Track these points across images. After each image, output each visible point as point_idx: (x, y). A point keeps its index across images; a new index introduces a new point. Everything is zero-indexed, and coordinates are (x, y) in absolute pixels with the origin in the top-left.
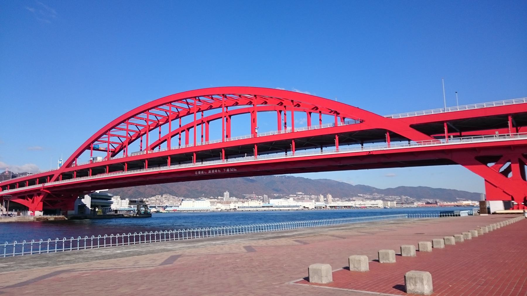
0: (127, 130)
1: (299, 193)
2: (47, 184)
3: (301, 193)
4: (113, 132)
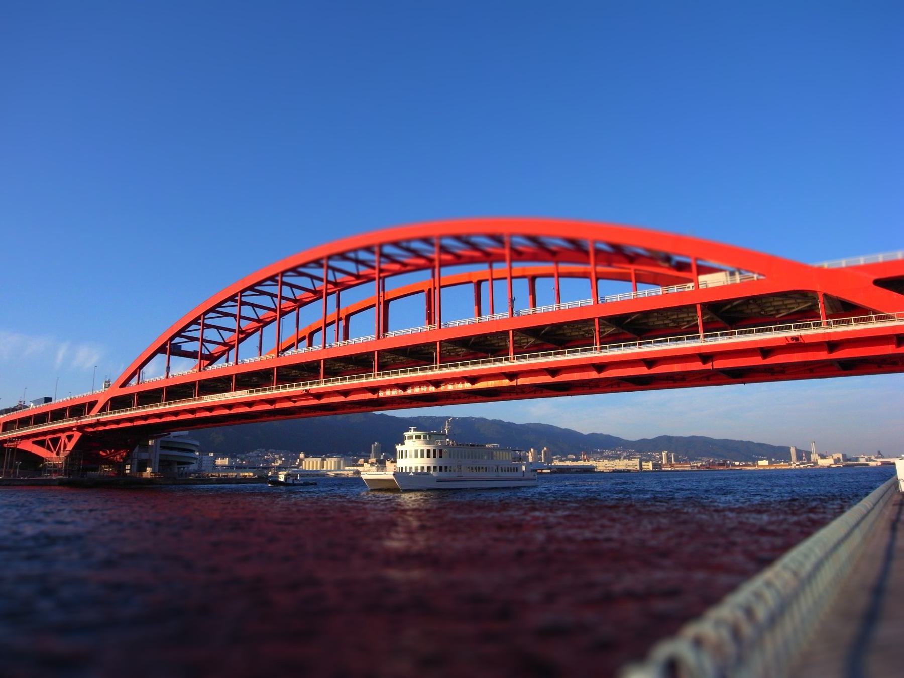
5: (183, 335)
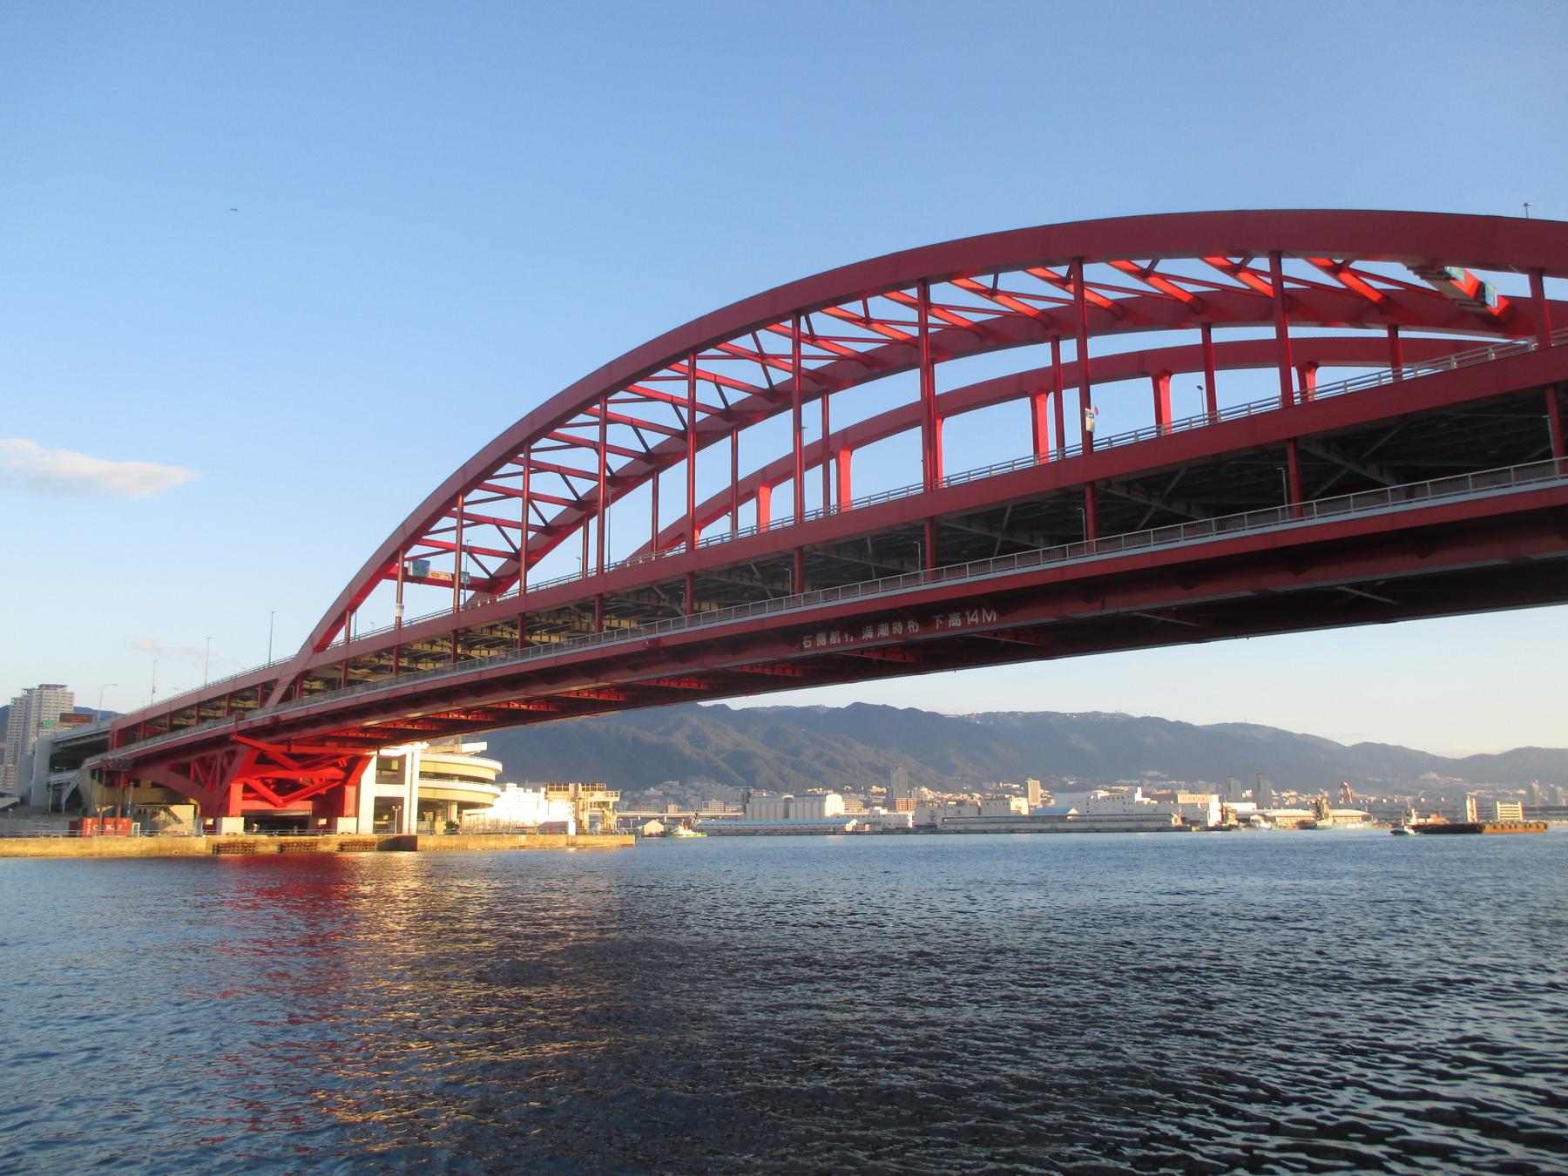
0: (602, 447)
1: (1150, 773)
2: (968, 1123)
5: (559, 434)
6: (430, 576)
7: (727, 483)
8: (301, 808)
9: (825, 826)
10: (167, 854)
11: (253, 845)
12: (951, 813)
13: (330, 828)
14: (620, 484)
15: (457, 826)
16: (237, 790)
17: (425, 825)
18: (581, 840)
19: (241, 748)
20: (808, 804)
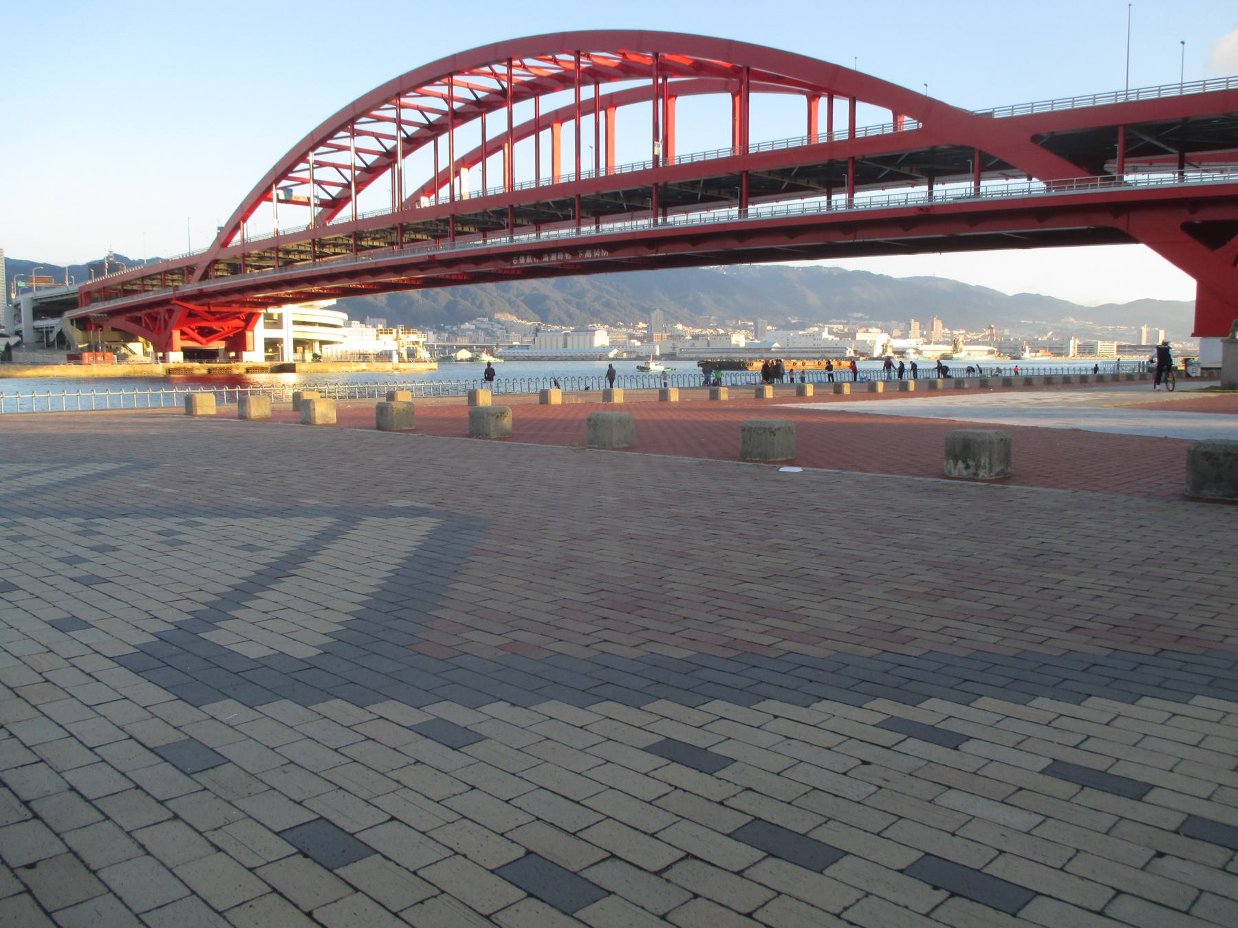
0: (399, 122)
3: (860, 315)
4: (363, 125)
6: (294, 199)
7: (479, 143)
8: (219, 345)
9: (594, 354)
10: (140, 375)
11: (191, 369)
12: (687, 345)
13: (238, 358)
14: (412, 143)
15: (320, 357)
16: (176, 334)
17: (299, 356)
18: (402, 366)
19: (176, 308)
20: (581, 338)
